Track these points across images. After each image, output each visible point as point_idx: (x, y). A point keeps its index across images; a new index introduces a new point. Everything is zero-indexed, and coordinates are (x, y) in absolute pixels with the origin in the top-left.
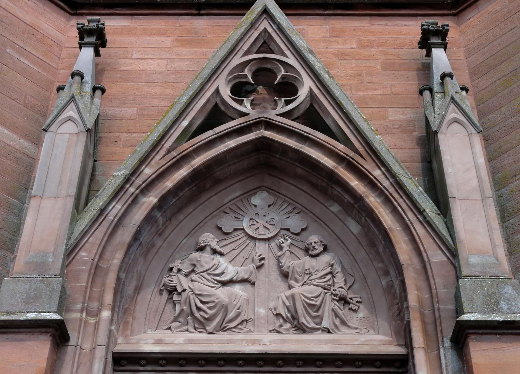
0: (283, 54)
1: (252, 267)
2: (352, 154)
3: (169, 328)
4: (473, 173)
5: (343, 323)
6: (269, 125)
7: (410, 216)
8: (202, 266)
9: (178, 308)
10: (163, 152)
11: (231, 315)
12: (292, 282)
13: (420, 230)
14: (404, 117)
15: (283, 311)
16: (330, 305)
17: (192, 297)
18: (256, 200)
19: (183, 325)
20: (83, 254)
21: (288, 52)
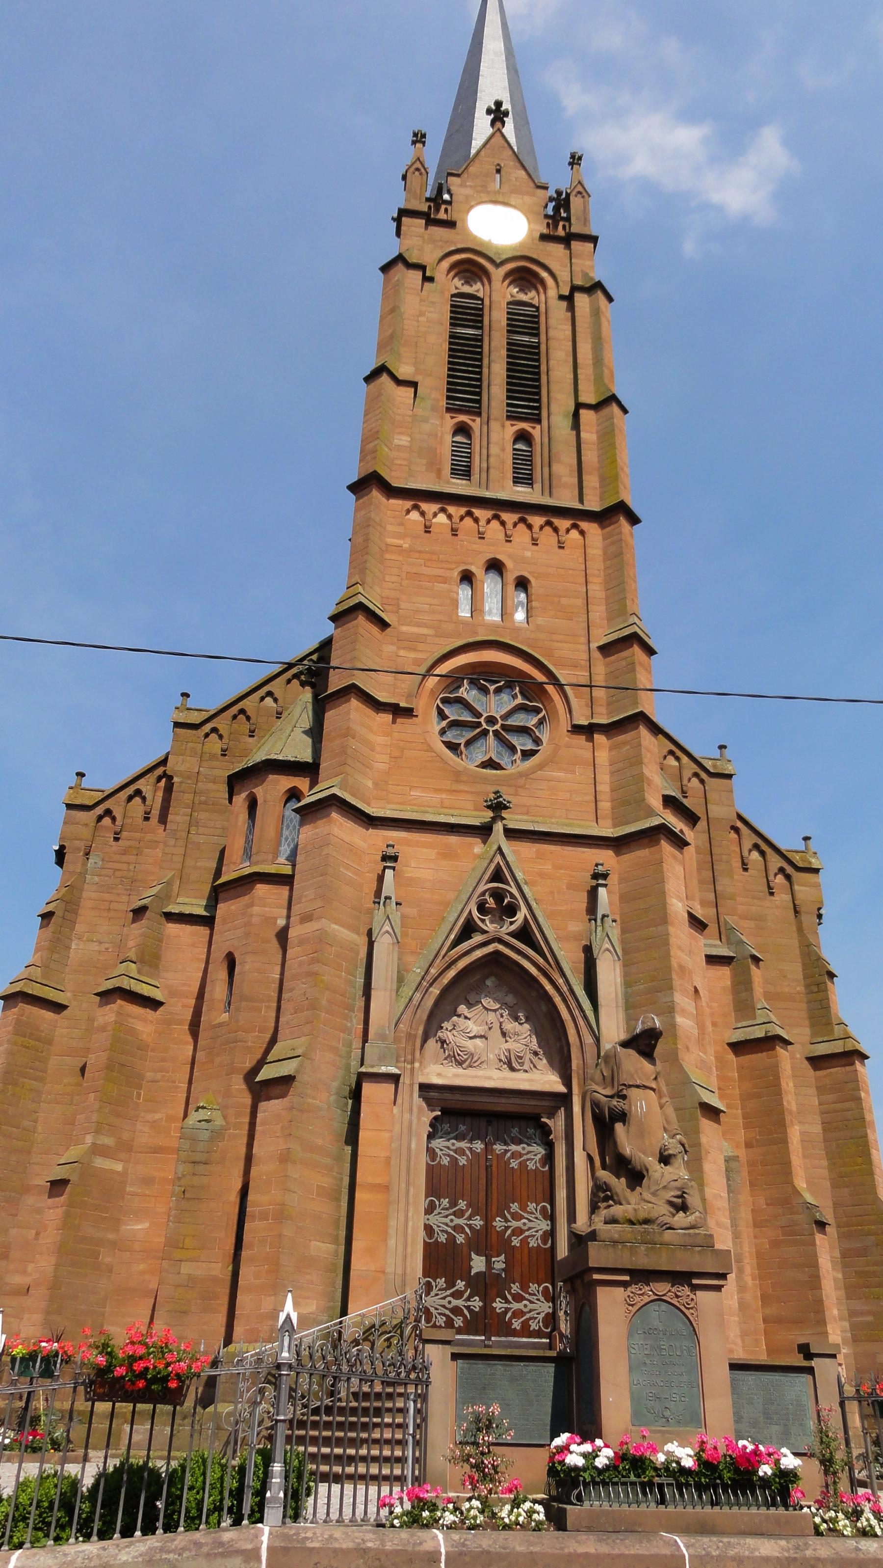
0: (509, 884)
1: (486, 1028)
2: (548, 966)
3: (442, 1064)
4: (613, 989)
5: (535, 1067)
6: (500, 941)
7: (577, 1012)
8: (460, 1027)
9: (447, 1054)
10: (441, 957)
11: (475, 1059)
12: (508, 1038)
13: (581, 1022)
14: (577, 929)
15: (503, 1058)
16: (529, 1056)
17: (455, 1047)
18: (489, 983)
19: (449, 1063)
20: (401, 1026)
21: (512, 884)
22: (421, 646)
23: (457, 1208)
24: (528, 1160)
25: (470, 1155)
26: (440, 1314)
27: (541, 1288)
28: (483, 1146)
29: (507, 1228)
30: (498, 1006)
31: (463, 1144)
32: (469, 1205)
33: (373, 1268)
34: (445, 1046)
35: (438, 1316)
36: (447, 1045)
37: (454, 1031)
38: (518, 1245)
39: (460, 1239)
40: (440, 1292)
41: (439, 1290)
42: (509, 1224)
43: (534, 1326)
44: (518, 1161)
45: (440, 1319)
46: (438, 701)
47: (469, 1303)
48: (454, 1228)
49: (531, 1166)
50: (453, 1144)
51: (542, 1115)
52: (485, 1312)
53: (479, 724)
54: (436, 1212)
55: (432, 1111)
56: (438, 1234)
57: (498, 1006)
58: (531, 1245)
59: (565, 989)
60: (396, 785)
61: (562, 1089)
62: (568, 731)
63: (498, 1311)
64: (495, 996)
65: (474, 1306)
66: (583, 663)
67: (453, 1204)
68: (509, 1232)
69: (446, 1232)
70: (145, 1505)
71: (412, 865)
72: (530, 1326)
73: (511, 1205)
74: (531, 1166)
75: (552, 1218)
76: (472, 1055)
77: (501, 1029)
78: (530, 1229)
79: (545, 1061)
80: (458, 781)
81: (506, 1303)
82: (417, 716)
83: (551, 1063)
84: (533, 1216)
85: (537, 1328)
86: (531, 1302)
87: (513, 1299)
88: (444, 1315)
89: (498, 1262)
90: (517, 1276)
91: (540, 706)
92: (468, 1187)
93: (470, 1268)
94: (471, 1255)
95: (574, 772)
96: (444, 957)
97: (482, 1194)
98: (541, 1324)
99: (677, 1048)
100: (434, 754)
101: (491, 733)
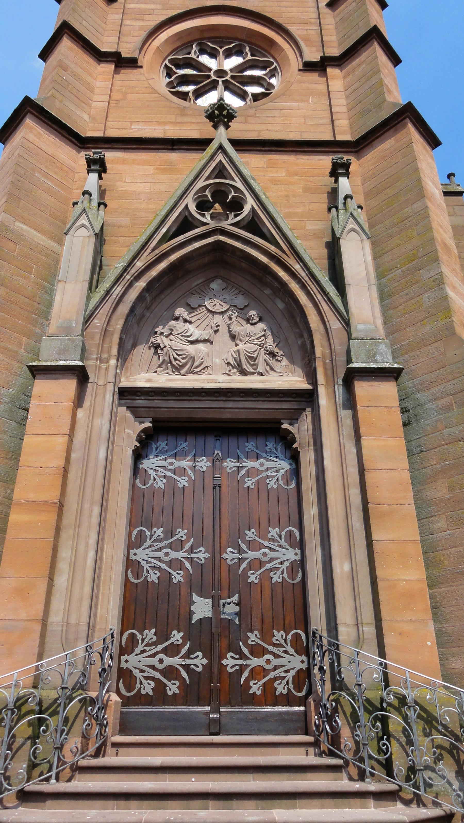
0: (233, 179)
1: (211, 331)
2: (280, 253)
3: (156, 372)
4: (363, 268)
5: (272, 369)
6: (223, 232)
7: (319, 297)
8: (177, 330)
10: (149, 251)
11: (196, 364)
12: (238, 342)
13: (325, 307)
14: (317, 227)
16: (263, 357)
18: (214, 285)
19: (165, 370)
20: (96, 321)
21: (236, 179)
22: (146, 17)
23: (175, 538)
24: (268, 477)
25: (192, 475)
26: (147, 678)
27: (289, 637)
28: (209, 464)
29: (241, 560)
30: (226, 307)
31: (184, 463)
32: (191, 535)
33: (23, 616)
34: (159, 351)
35: (144, 681)
36: (162, 349)
37: (171, 337)
38: (257, 581)
39: (178, 577)
40: (147, 648)
41: (147, 645)
42: (244, 555)
43: (281, 689)
44: (254, 480)
45: (146, 685)
46: (167, 62)
47: (188, 661)
48: (170, 564)
49: (272, 484)
50: (171, 464)
51: (282, 421)
52: (211, 673)
53: (209, 77)
54: (146, 545)
55: (141, 423)
56: (148, 572)
57: (226, 307)
58: (274, 581)
59: (303, 274)
60: (116, 121)
61: (306, 386)
62: (300, 70)
63: (230, 670)
64: (222, 298)
65: (195, 665)
66: (313, 20)
67: (170, 533)
68: (244, 565)
69: (159, 569)
70: (280, 713)
71: (127, 180)
72: (276, 689)
73: (247, 532)
74: (272, 484)
75: (301, 545)
76: (193, 359)
77: (230, 332)
78: (271, 560)
79: (285, 362)
80: (183, 115)
81: (240, 658)
82: (141, 67)
83: (292, 361)
84: (276, 544)
85: (285, 692)
86: (276, 656)
87: (252, 653)
88: (153, 679)
89: (229, 604)
90: (256, 622)
91: (272, 60)
92: (188, 511)
93: (191, 613)
94: (191, 597)
95: (308, 102)
96: (153, 250)
97: (208, 521)
98: (291, 686)
99: (453, 321)
100: (159, 96)
101: (220, 83)
